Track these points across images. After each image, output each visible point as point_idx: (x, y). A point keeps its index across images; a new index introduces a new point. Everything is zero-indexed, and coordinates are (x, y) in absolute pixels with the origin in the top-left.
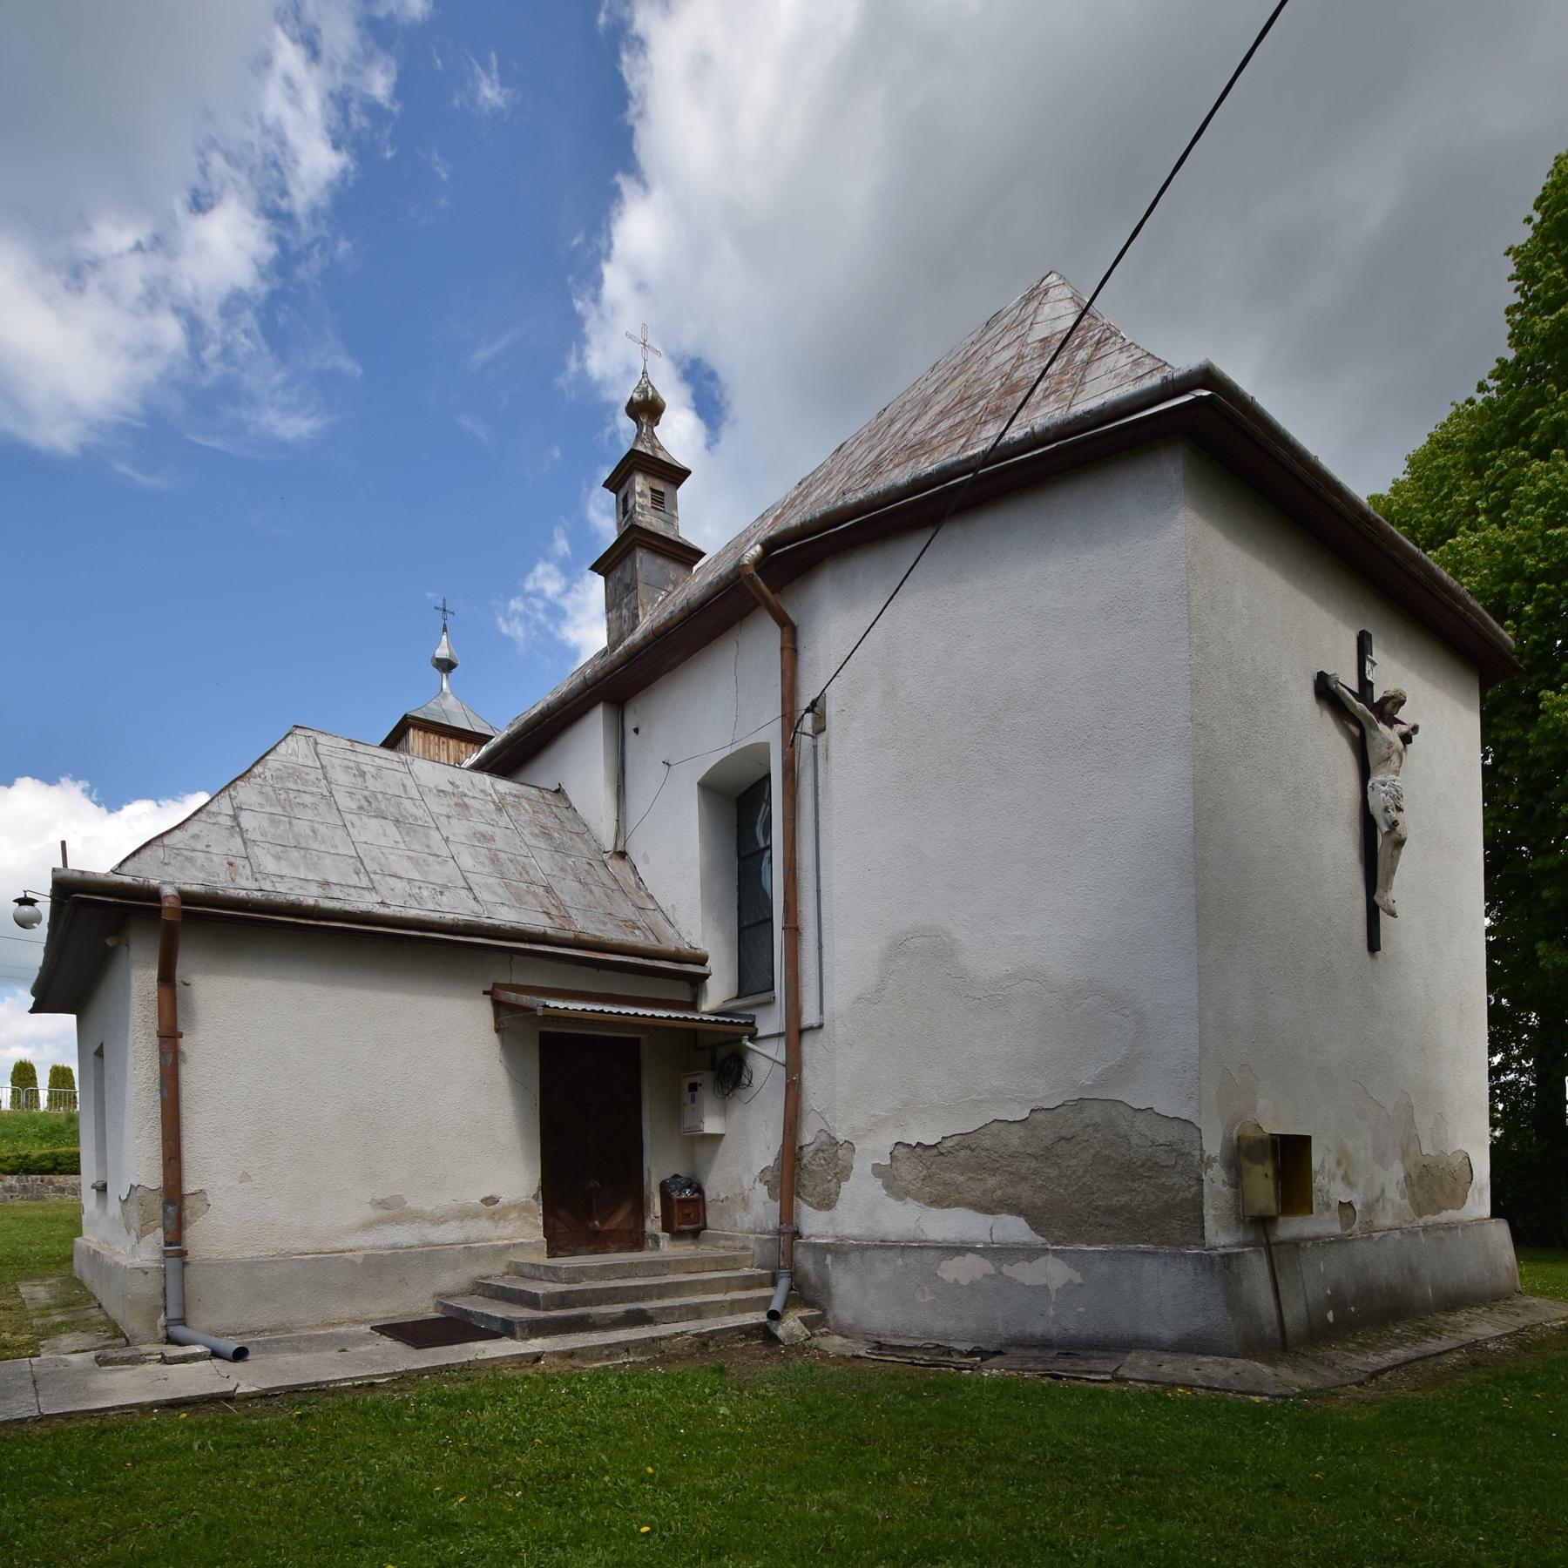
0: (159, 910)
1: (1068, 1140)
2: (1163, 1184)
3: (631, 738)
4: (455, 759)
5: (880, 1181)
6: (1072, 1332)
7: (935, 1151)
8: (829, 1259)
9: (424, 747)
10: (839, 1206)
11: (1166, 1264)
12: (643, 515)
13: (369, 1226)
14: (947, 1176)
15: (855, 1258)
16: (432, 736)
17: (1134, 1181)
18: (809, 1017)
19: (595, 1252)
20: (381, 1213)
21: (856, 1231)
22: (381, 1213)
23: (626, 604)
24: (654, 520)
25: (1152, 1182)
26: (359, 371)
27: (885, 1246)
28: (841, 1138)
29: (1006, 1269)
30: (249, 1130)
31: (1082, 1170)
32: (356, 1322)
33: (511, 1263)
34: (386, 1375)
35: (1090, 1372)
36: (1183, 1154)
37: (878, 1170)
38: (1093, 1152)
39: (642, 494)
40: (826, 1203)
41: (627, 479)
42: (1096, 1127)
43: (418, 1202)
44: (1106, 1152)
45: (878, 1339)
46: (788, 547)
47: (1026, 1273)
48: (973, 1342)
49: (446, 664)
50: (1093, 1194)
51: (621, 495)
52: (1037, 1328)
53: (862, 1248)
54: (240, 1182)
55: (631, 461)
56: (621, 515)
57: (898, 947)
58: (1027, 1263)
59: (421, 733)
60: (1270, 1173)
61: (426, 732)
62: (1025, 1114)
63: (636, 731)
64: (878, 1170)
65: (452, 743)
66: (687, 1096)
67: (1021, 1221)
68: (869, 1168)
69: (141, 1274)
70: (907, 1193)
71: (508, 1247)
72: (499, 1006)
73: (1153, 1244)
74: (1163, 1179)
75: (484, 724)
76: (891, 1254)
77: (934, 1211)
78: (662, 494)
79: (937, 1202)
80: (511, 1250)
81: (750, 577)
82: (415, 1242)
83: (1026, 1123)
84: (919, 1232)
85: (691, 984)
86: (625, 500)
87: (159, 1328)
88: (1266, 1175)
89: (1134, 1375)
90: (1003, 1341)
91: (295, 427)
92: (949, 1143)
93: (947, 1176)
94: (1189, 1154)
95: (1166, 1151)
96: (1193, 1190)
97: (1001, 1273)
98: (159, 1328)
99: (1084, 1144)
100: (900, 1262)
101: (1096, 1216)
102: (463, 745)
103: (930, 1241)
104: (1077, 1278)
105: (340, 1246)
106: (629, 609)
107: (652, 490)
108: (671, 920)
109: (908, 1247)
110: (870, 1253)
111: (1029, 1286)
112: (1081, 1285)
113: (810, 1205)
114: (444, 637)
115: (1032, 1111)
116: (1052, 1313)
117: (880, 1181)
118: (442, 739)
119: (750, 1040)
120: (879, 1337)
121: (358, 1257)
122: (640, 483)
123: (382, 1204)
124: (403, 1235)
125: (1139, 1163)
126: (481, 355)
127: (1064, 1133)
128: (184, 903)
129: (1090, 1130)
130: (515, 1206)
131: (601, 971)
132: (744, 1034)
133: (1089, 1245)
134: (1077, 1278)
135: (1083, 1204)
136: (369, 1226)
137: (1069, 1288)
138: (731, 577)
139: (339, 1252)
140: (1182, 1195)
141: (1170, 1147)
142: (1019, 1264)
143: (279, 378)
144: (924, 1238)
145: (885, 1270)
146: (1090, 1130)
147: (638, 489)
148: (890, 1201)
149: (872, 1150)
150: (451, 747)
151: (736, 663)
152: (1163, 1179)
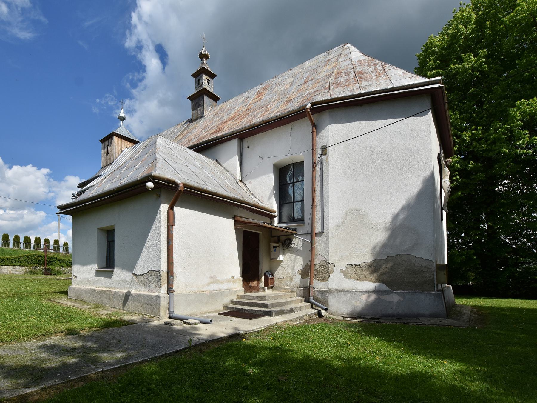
0: (178, 188)
1: (397, 264)
2: (424, 276)
3: (245, 150)
4: (126, 146)
5: (342, 274)
6: (400, 313)
7: (359, 266)
8: (328, 294)
9: (118, 142)
10: (329, 280)
11: (426, 295)
12: (205, 85)
13: (209, 284)
14: (362, 273)
15: (336, 294)
16: (120, 139)
17: (416, 275)
18: (318, 229)
19: (151, 295)
20: (212, 280)
21: (334, 287)
22: (212, 280)
23: (199, 110)
24: (208, 87)
25: (421, 275)
26: (47, 22)
27: (344, 291)
28: (330, 262)
29: (381, 297)
30: (185, 254)
31: (401, 272)
32: (213, 312)
33: (238, 295)
34: (264, 327)
35: (416, 323)
36: (429, 268)
37: (342, 271)
38: (405, 267)
39: (205, 80)
40: (325, 279)
41: (200, 75)
42: (405, 261)
43: (219, 278)
44: (408, 267)
45: (343, 316)
46: (319, 106)
47: (387, 298)
48: (371, 316)
49: (123, 118)
50: (405, 278)
51: (197, 79)
52: (390, 312)
53: (338, 292)
54: (184, 270)
55: (202, 70)
56: (197, 85)
57: (348, 213)
58: (387, 295)
59: (117, 138)
60: (445, 273)
61: (118, 138)
62: (386, 257)
63: (248, 147)
64: (342, 271)
65: (125, 141)
66: (272, 249)
67: (384, 285)
68: (339, 271)
69: (164, 298)
70: (351, 277)
71: (237, 291)
72: (235, 221)
73: (421, 290)
74: (424, 275)
75: (134, 137)
76: (347, 293)
77: (359, 282)
78: (209, 80)
79: (360, 279)
80: (238, 292)
81: (308, 112)
82: (218, 289)
83: (386, 260)
84: (354, 287)
85: (270, 219)
86: (199, 80)
87: (167, 314)
88: (444, 274)
89: (427, 323)
90: (380, 315)
91: (25, 35)
92: (363, 264)
93: (362, 273)
94: (431, 268)
95: (425, 268)
96: (432, 277)
97: (380, 298)
98: (167, 314)
99: (402, 265)
100: (349, 295)
101: (405, 284)
102: (128, 142)
103: (357, 290)
104: (402, 299)
105: (203, 290)
106: (200, 111)
107: (207, 79)
108: (261, 200)
109: (352, 291)
110: (340, 293)
111: (388, 301)
112: (402, 301)
113: (318, 280)
114: (122, 110)
115: (388, 257)
116: (394, 308)
117: (342, 274)
118: (123, 140)
119: (295, 235)
120: (343, 315)
121: (208, 293)
122: (204, 77)
123: (212, 278)
124: (215, 287)
125: (417, 271)
126: (87, 24)
127: (396, 262)
128: (184, 187)
129: (404, 262)
130: (237, 279)
131: (254, 214)
132: (295, 233)
133: (403, 291)
134: (402, 299)
135: (402, 280)
136: (209, 284)
137: (399, 302)
138: (297, 111)
139: (203, 292)
140: (429, 278)
141: (426, 267)
142: (385, 295)
143: (20, 19)
144: (356, 289)
145: (344, 297)
146: (404, 262)
147: (204, 78)
148: (346, 279)
149: (343, 265)
150: (125, 143)
151: (291, 134)
152: (424, 275)
